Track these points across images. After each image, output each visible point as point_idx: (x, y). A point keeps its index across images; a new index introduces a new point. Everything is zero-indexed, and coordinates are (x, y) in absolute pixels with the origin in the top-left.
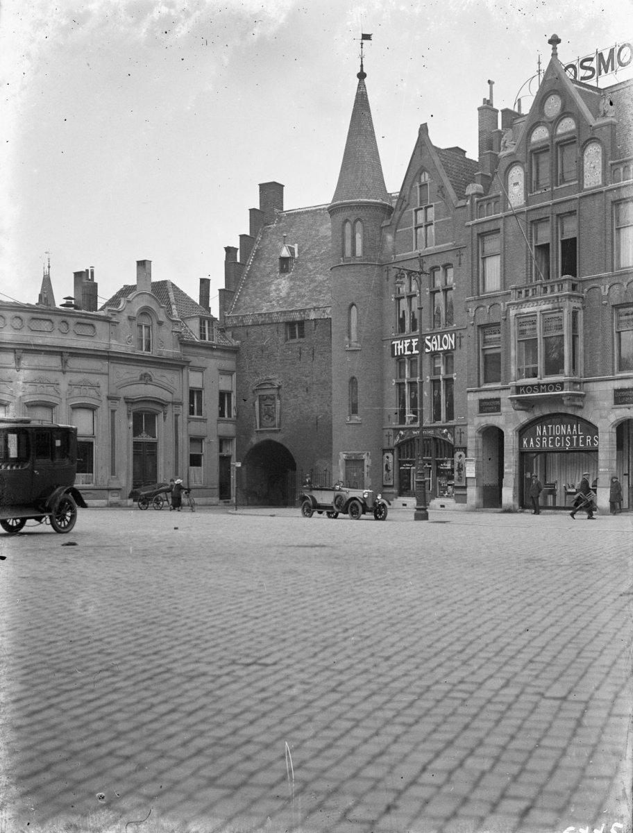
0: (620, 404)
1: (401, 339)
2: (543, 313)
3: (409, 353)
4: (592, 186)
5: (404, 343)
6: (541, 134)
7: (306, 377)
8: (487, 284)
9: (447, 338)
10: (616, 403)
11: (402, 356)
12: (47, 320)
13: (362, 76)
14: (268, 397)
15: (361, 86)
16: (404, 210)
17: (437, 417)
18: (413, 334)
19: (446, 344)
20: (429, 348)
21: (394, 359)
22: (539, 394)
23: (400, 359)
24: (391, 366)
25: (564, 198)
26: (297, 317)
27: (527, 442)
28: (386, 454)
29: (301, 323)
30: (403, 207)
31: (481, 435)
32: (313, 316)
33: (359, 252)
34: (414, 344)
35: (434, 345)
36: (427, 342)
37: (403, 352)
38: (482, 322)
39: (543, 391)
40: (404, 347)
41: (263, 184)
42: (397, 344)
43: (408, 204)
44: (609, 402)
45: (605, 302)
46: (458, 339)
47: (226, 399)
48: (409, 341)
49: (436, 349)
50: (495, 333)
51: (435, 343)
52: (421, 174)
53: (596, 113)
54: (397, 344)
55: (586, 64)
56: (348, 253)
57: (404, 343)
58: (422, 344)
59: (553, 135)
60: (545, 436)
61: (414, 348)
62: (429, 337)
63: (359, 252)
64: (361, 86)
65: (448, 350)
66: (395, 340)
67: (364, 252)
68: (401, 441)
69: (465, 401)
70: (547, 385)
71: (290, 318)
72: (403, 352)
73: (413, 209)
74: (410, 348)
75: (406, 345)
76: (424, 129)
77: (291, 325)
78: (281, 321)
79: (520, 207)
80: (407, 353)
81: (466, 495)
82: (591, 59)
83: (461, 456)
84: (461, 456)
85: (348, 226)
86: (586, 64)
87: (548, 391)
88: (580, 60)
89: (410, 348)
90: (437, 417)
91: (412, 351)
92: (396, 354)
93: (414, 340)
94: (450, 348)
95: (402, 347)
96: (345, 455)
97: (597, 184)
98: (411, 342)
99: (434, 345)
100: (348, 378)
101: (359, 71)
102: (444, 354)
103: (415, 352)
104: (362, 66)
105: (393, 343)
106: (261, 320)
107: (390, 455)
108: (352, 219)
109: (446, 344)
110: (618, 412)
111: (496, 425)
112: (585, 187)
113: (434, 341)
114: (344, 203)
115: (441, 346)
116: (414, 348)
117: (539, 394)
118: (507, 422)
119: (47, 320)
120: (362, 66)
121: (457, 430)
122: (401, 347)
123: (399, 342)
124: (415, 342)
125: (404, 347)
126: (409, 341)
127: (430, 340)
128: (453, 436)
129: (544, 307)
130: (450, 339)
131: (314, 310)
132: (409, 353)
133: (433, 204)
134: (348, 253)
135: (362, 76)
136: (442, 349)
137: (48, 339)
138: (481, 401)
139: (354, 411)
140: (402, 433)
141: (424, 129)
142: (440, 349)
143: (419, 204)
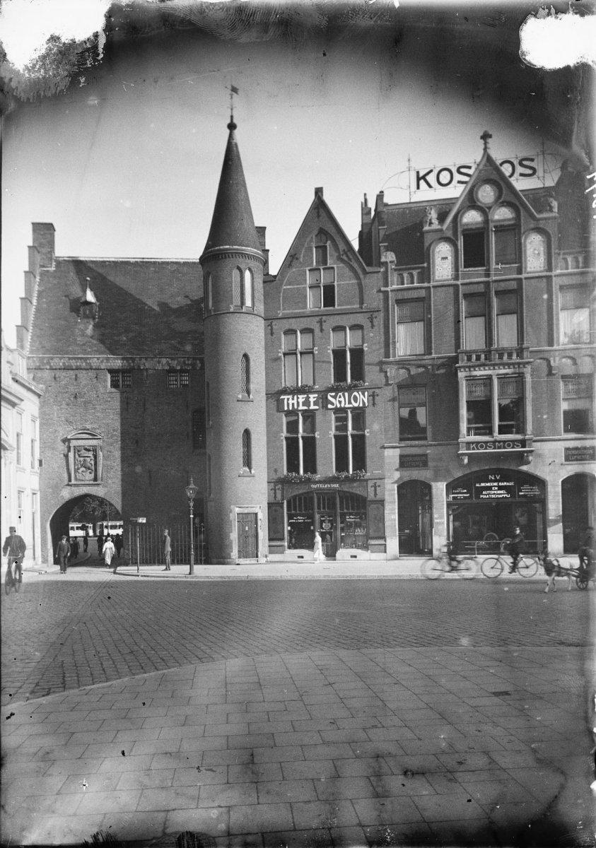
0: (570, 461)
2: (502, 378)
4: (440, 278)
5: (298, 398)
8: (463, 340)
9: (358, 396)
10: (567, 459)
13: (232, 127)
19: (356, 401)
20: (333, 404)
22: (493, 450)
25: (504, 277)
35: (340, 402)
36: (329, 398)
37: (296, 407)
39: (499, 448)
41: (39, 224)
42: (288, 399)
47: (481, 425)
49: (343, 405)
51: (342, 399)
54: (288, 399)
61: (312, 403)
62: (333, 394)
64: (231, 136)
65: (358, 408)
69: (382, 457)
70: (504, 442)
72: (296, 407)
74: (307, 403)
75: (301, 400)
76: (319, 192)
79: (540, 272)
80: (301, 407)
81: (270, 540)
82: (469, 167)
87: (505, 448)
88: (458, 166)
89: (307, 403)
91: (309, 406)
93: (312, 396)
94: (361, 405)
95: (295, 402)
98: (308, 398)
99: (340, 402)
103: (312, 407)
104: (232, 117)
109: (356, 401)
110: (570, 468)
111: (423, 479)
113: (340, 397)
115: (350, 403)
116: (312, 403)
117: (493, 450)
120: (232, 117)
123: (290, 397)
127: (335, 397)
129: (503, 371)
130: (362, 396)
132: (305, 408)
135: (232, 127)
136: (351, 406)
138: (567, 449)
141: (319, 192)
142: (347, 406)
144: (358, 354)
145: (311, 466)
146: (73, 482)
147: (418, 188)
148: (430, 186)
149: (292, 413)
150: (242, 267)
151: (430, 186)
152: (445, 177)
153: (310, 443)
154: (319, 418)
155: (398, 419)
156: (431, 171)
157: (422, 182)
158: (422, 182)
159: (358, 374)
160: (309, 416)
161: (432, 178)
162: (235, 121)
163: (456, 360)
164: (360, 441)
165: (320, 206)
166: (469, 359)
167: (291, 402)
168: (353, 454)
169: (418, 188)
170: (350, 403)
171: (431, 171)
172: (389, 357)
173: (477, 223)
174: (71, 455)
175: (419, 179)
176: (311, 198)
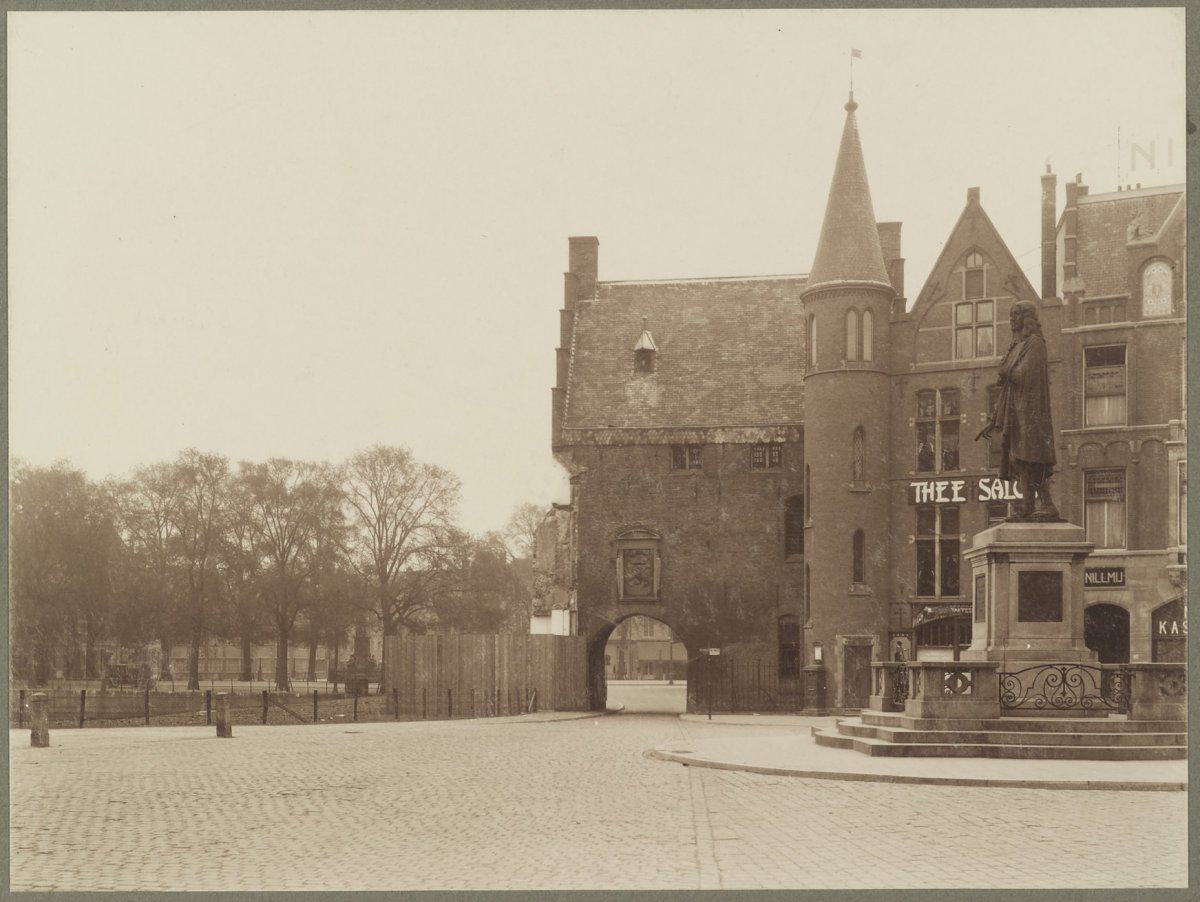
1: (929, 480)
3: (946, 500)
5: (936, 486)
7: (707, 525)
11: (931, 504)
13: (851, 107)
14: (639, 552)
16: (936, 302)
17: (926, 587)
18: (953, 473)
20: (986, 495)
23: (926, 511)
24: (910, 518)
26: (693, 438)
27: (1165, 626)
28: (896, 639)
29: (696, 449)
30: (934, 298)
31: (491, 609)
32: (720, 438)
33: (868, 354)
35: (997, 492)
37: (932, 498)
40: (936, 492)
42: (921, 488)
43: (944, 295)
45: (1074, 464)
48: (947, 483)
49: (1000, 497)
50: (1110, 482)
52: (970, 254)
54: (921, 488)
56: (852, 354)
57: (936, 486)
58: (972, 490)
62: (987, 480)
63: (868, 354)
64: (850, 120)
66: (913, 480)
67: (874, 357)
68: (925, 621)
71: (675, 438)
72: (932, 498)
73: (954, 303)
74: (948, 493)
75: (940, 489)
76: (974, 195)
77: (676, 449)
78: (664, 442)
80: (940, 499)
85: (852, 317)
89: (948, 493)
90: (926, 587)
92: (918, 500)
93: (954, 483)
95: (931, 491)
96: (845, 640)
97: (1164, 313)
98: (950, 486)
99: (997, 492)
101: (847, 101)
102: (941, 508)
103: (956, 499)
105: (913, 484)
106: (627, 438)
108: (860, 307)
112: (1145, 314)
113: (997, 485)
114: (850, 284)
118: (1137, 599)
120: (851, 93)
122: (928, 491)
123: (925, 484)
124: (957, 486)
125: (936, 492)
126: (947, 483)
127: (989, 485)
131: (723, 430)
132: (946, 500)
133: (994, 299)
134: (852, 354)
135: (851, 107)
136: (1013, 497)
137: (1104, 380)
139: (858, 576)
140: (929, 610)
141: (974, 195)
142: (1007, 497)
143: (964, 295)
162: (856, 99)
165: (974, 218)
176: (962, 203)
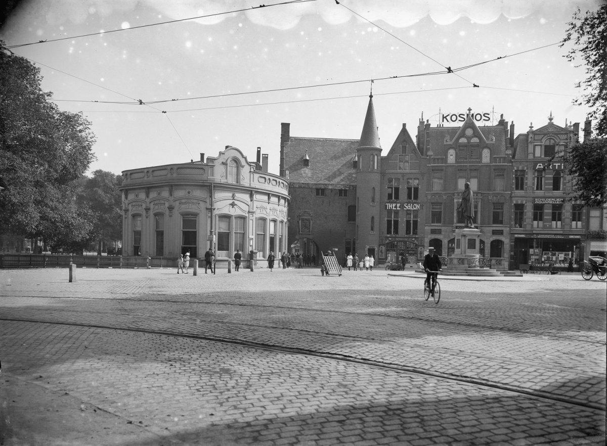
6: (463, 140)
11: (391, 209)
12: (201, 168)
13: (371, 96)
15: (371, 100)
19: (415, 207)
21: (386, 211)
32: (330, 187)
34: (398, 206)
38: (433, 201)
44: (490, 234)
46: (422, 206)
53: (488, 139)
55: (461, 116)
58: (402, 206)
59: (469, 142)
60: (19, 258)
64: (371, 100)
67: (377, 168)
71: (319, 187)
74: (396, 207)
75: (394, 206)
76: (404, 125)
77: (318, 190)
80: (394, 209)
83: (421, 249)
84: (421, 249)
86: (461, 116)
89: (396, 207)
100: (371, 217)
103: (398, 209)
107: (383, 247)
109: (415, 207)
110: (494, 237)
115: (413, 208)
119: (201, 168)
121: (420, 239)
127: (407, 205)
128: (417, 241)
135: (371, 96)
141: (404, 125)
144: (416, 189)
145: (396, 232)
146: (301, 233)
147: (443, 121)
148: (448, 121)
149: (390, 211)
150: (374, 154)
151: (448, 121)
152: (454, 118)
153: (396, 222)
154: (400, 213)
155: (124, 240)
156: (449, 115)
157: (445, 119)
158: (445, 119)
159: (416, 197)
160: (397, 212)
161: (448, 118)
163: (453, 194)
164: (415, 223)
165: (404, 132)
166: (458, 195)
167: (390, 206)
168: (413, 228)
169: (443, 121)
170: (413, 208)
171: (449, 115)
172: (492, 243)
173: (465, 143)
174: (300, 221)
175: (443, 118)
